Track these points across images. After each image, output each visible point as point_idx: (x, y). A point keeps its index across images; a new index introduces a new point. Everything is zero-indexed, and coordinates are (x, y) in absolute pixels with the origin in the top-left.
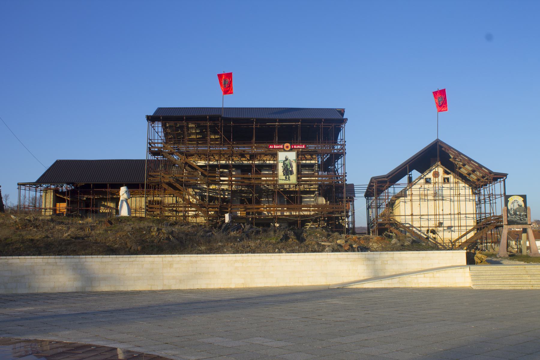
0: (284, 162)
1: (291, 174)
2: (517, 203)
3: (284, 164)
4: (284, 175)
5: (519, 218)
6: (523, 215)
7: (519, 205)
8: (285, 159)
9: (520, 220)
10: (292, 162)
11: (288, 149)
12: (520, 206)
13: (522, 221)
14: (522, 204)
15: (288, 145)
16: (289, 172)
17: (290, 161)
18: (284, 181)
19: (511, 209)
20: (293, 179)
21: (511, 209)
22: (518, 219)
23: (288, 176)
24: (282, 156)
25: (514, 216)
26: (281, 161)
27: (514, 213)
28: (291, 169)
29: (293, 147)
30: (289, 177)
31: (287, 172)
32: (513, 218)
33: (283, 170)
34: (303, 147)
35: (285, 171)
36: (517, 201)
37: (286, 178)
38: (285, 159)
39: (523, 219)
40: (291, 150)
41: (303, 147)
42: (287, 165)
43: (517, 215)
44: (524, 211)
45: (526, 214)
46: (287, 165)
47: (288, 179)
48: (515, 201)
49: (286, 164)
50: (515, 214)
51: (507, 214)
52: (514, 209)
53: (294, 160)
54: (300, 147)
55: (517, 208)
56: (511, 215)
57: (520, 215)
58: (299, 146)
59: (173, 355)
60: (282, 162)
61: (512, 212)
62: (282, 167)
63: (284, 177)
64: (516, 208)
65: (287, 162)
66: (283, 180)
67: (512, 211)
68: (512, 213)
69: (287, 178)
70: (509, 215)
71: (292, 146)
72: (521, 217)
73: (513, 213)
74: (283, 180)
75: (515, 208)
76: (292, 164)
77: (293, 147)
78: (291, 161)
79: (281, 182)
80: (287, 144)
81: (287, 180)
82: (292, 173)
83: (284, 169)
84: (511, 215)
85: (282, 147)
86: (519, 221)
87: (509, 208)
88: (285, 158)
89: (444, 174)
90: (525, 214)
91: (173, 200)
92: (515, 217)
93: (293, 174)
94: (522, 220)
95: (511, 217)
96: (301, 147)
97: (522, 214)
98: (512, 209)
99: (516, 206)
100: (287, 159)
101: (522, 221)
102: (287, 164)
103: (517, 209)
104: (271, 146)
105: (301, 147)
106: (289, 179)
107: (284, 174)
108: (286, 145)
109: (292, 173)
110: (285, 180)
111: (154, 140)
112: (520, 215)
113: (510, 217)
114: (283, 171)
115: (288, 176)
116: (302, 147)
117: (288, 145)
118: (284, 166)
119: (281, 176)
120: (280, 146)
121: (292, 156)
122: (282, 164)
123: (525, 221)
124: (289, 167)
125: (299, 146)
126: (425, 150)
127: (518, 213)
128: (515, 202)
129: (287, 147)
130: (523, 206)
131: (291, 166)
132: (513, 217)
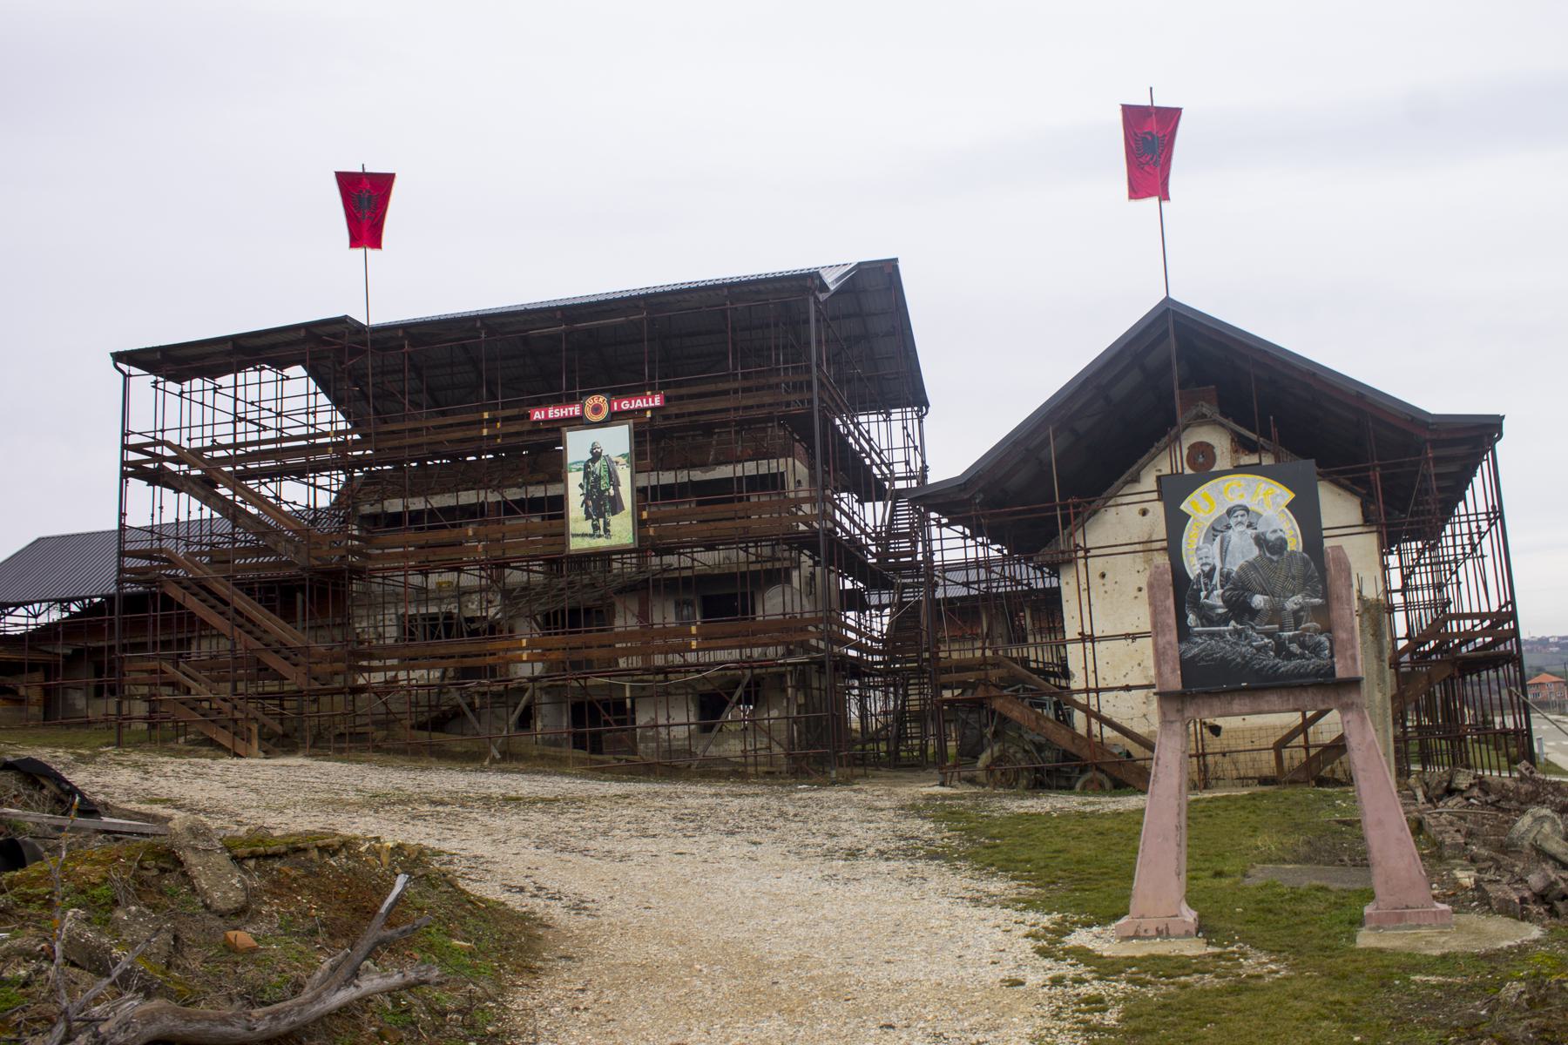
0: (586, 466)
1: (614, 513)
2: (1250, 525)
3: (586, 476)
4: (588, 516)
5: (1269, 635)
6: (1295, 613)
7: (1260, 541)
8: (590, 456)
9: (1281, 649)
10: (617, 463)
11: (600, 418)
12: (1271, 547)
13: (1290, 656)
14: (1290, 532)
15: (601, 400)
16: (605, 505)
17: (610, 460)
18: (587, 539)
19: (1209, 575)
20: (621, 530)
21: (1209, 575)
22: (1259, 649)
23: (601, 521)
24: (577, 445)
25: (1233, 623)
26: (576, 463)
27: (1227, 602)
28: (612, 492)
29: (619, 406)
30: (607, 524)
31: (601, 504)
32: (1228, 640)
33: (583, 497)
34: (653, 402)
35: (590, 503)
36: (1246, 509)
37: (596, 528)
38: (590, 456)
39: (1303, 645)
40: (614, 418)
41: (653, 402)
42: (599, 478)
43: (1254, 613)
44: (1307, 579)
45: (1317, 601)
46: (599, 478)
47: (602, 533)
48: (1230, 512)
49: (593, 473)
50: (1239, 608)
51: (1181, 618)
52: (1226, 577)
53: (623, 456)
54: (646, 405)
55: (1251, 565)
56: (1211, 623)
57: (1276, 613)
58: (639, 401)
59: (1344, 977)
60: (579, 470)
61: (1216, 599)
62: (581, 486)
63: (587, 527)
64: (1242, 562)
65: (597, 465)
66: (584, 535)
67: (1219, 591)
68: (1213, 607)
69: (599, 528)
70: (1192, 619)
71: (615, 404)
72: (1282, 630)
73: (1220, 603)
74: (584, 535)
75: (1234, 566)
76: (615, 472)
77: (619, 406)
78: (614, 459)
79: (576, 545)
80: (596, 397)
81: (600, 536)
82: (616, 506)
83: (588, 496)
84: (1206, 616)
85: (577, 413)
86: (1270, 660)
87: (1193, 568)
88: (592, 452)
89: (1236, 451)
90: (1315, 608)
91: (1085, 648)
92: (1236, 631)
93: (622, 508)
94: (1294, 648)
95: (1211, 635)
96: (647, 403)
97: (1292, 603)
98: (1217, 578)
99: (1242, 550)
100: (596, 456)
101: (1290, 656)
102: (598, 472)
103: (1253, 575)
104: (537, 413)
105: (647, 403)
106: (607, 531)
107: (587, 512)
108: (591, 401)
109: (616, 506)
110: (591, 536)
111: (1445, 549)
112: (1276, 613)
113: (1200, 634)
114: (584, 502)
115: (601, 521)
116: (651, 404)
117: (601, 400)
118: (588, 483)
119: (576, 521)
120: (571, 409)
121: (616, 441)
122: (581, 473)
123: (1318, 656)
124: (604, 484)
125: (639, 401)
126: (1285, 364)
127: (1258, 601)
128: (1232, 522)
129: (597, 409)
130: (1295, 543)
131: (615, 483)
132: (1221, 635)
